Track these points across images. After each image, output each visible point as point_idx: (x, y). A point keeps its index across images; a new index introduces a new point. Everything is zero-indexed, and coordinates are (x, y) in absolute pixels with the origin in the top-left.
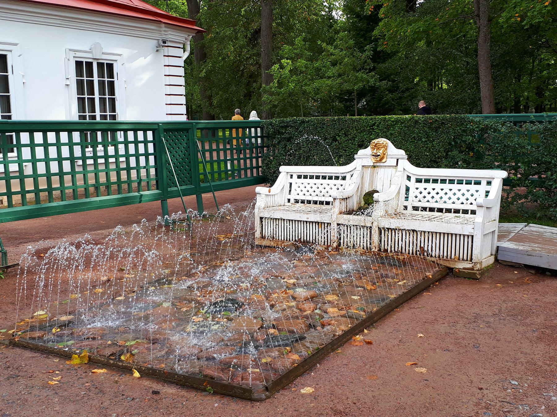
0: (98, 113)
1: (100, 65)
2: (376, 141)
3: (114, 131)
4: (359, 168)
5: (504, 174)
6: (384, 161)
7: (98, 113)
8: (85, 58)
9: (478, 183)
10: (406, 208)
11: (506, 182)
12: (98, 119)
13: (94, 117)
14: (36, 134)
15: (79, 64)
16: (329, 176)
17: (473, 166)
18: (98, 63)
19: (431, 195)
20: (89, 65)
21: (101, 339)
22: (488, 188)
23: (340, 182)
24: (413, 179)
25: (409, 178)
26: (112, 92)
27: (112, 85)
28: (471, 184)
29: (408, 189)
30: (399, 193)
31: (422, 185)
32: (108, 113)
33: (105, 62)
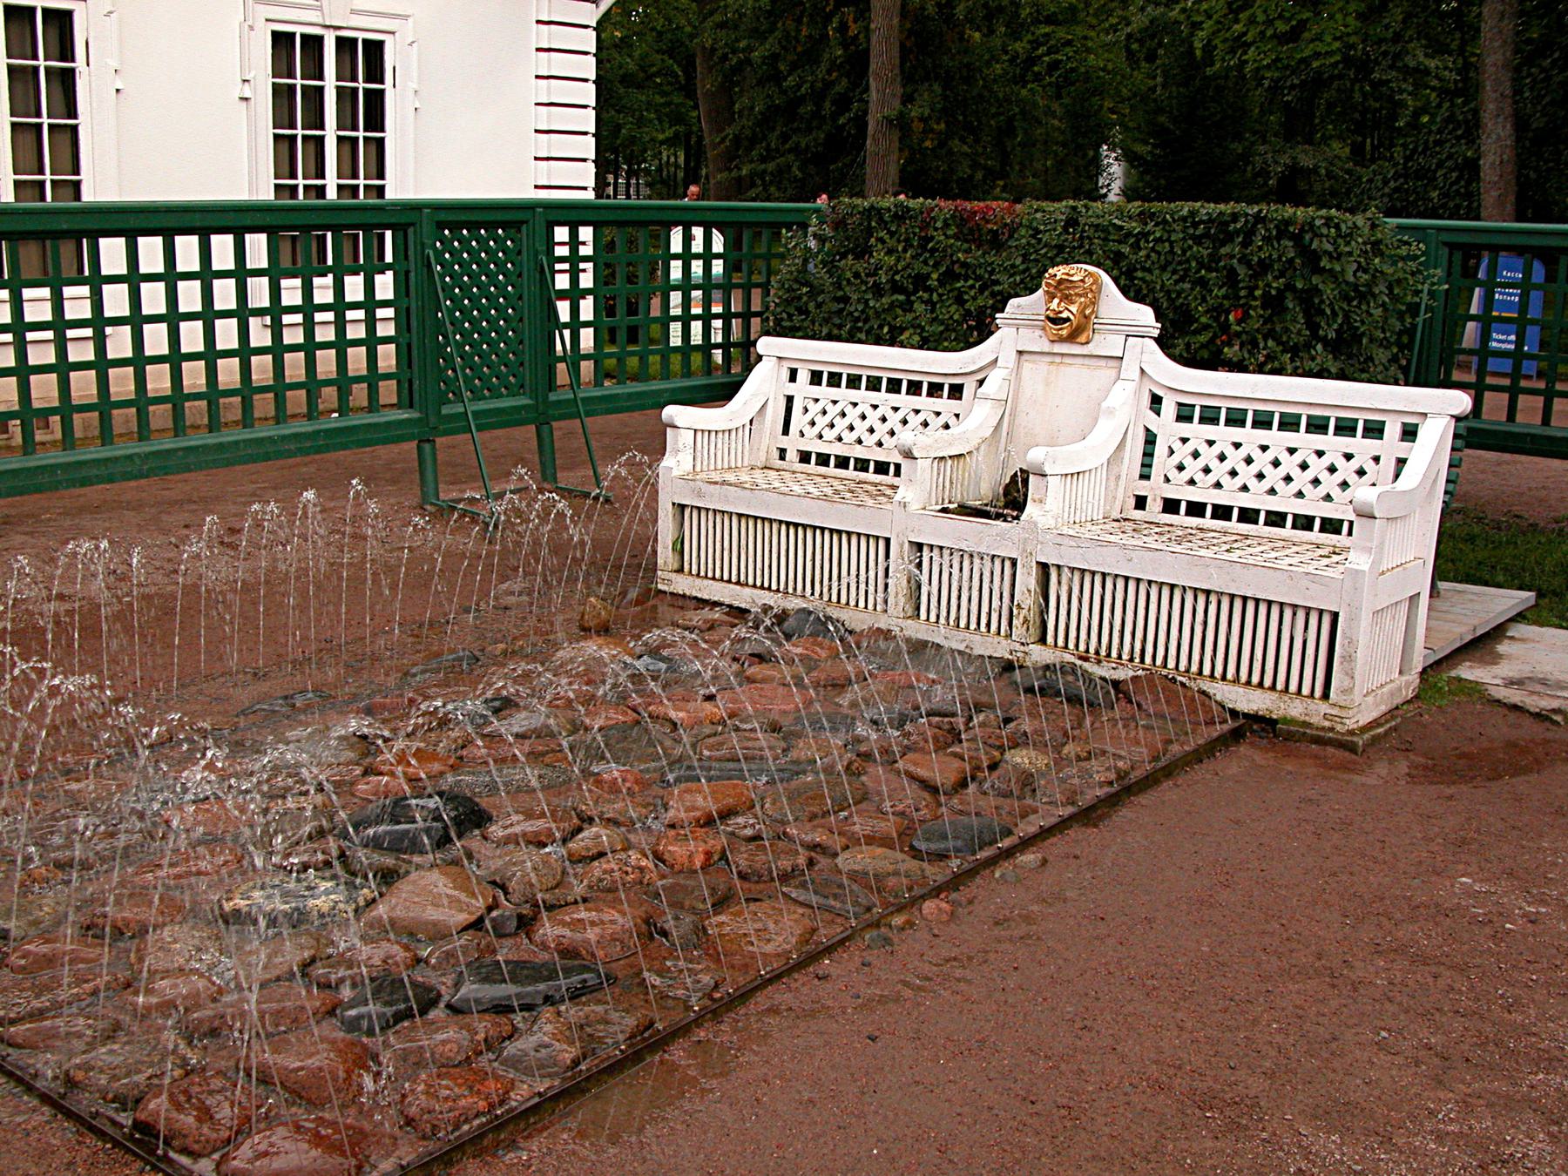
0: (331, 182)
1: (345, 46)
2: (1060, 271)
3: (373, 230)
4: (1008, 359)
5: (1460, 401)
6: (1082, 339)
7: (331, 182)
8: (301, 20)
9: (1375, 430)
10: (1141, 503)
11: (1469, 435)
12: (331, 194)
13: (320, 192)
14: (215, 239)
15: (281, 41)
16: (1282, 415)
17: (1269, 358)
18: (340, 40)
19: (1338, 477)
20: (313, 44)
21: (1270, 1075)
22: (1402, 449)
23: (944, 404)
24: (1169, 409)
25: (1156, 401)
26: (376, 119)
27: (376, 102)
28: (1242, 423)
29: (1150, 439)
30: (1121, 446)
31: (1196, 431)
32: (301, 182)
33: (361, 36)
